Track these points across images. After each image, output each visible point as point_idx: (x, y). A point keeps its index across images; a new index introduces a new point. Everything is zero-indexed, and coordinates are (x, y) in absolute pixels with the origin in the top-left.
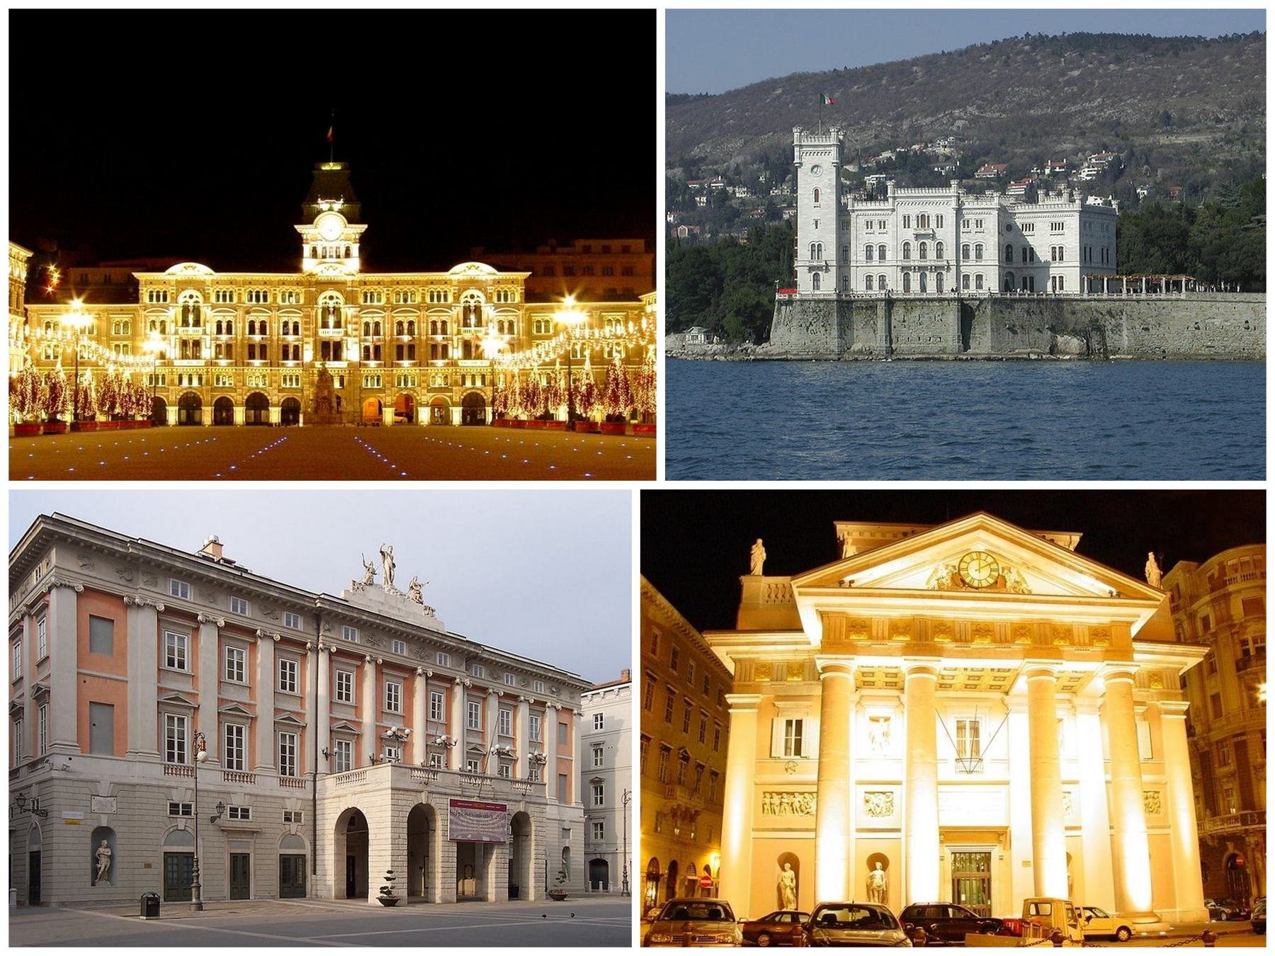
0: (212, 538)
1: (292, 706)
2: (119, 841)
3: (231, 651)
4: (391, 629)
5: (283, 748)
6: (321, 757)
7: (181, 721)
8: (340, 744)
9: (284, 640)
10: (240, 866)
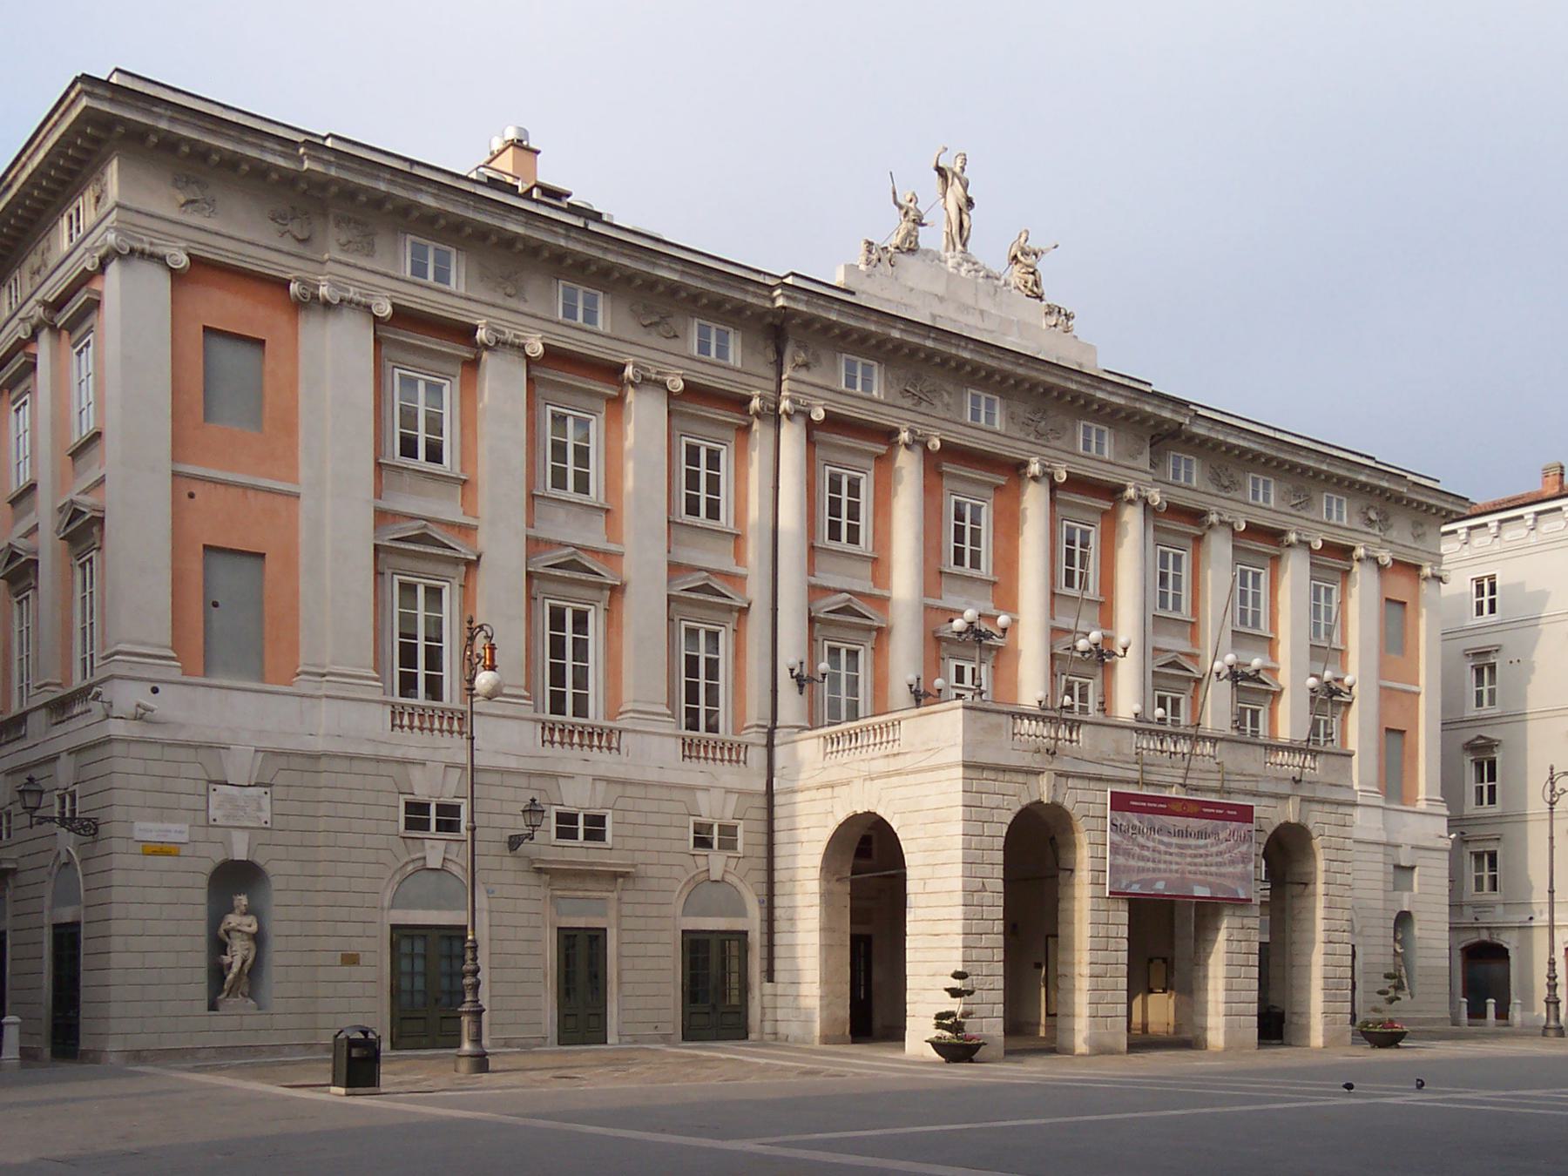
0: (511, 134)
2: (276, 898)
3: (559, 420)
4: (962, 363)
5: (692, 662)
6: (786, 684)
7: (434, 594)
8: (834, 652)
9: (694, 391)
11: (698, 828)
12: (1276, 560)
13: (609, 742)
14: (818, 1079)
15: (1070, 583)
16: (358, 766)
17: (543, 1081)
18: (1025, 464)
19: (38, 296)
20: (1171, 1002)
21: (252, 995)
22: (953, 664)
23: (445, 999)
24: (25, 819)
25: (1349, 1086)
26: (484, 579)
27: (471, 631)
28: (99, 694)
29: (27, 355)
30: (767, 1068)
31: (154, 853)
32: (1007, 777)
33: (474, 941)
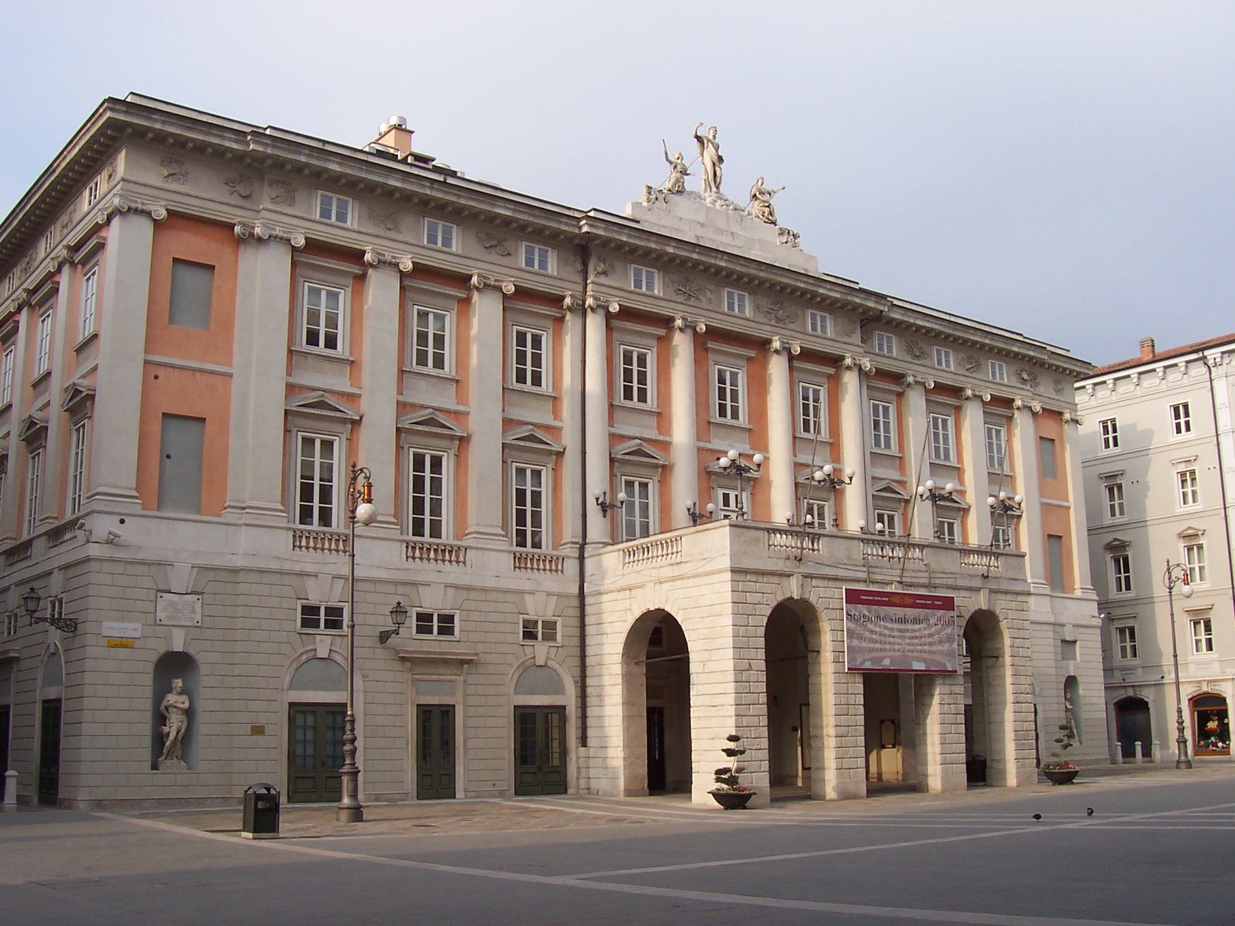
0: (394, 121)
1: (536, 414)
2: (204, 681)
3: (423, 316)
4: (719, 270)
5: (521, 494)
6: (593, 510)
7: (327, 446)
8: (629, 484)
9: (522, 293)
10: (436, 729)
11: (526, 624)
12: (958, 409)
13: (458, 557)
14: (623, 825)
15: (807, 429)
16: (267, 578)
17: (406, 829)
18: (769, 342)
19: (64, 243)
20: (899, 755)
21: (183, 758)
22: (720, 492)
23: (330, 763)
24: (27, 620)
25: (1038, 817)
26: (364, 432)
27: (354, 472)
28: (83, 525)
29: (53, 283)
30: (583, 816)
31: (116, 646)
32: (765, 579)
33: (352, 716)
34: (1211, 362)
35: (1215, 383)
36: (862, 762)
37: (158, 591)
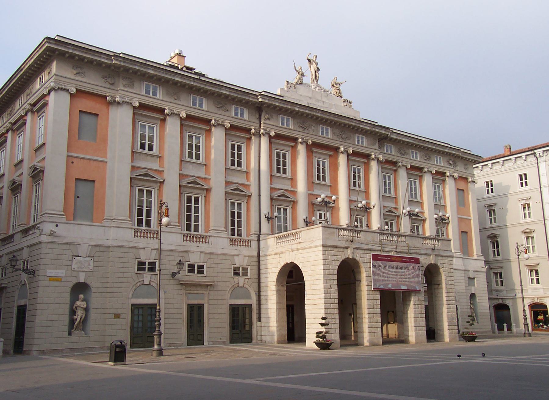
1: (239, 179)
2: (93, 295)
3: (191, 137)
4: (317, 117)
5: (233, 213)
7: (149, 193)
8: (279, 209)
10: (196, 314)
11: (235, 269)
12: (421, 177)
13: (206, 240)
14: (277, 356)
15: (355, 185)
17: (182, 359)
18: (339, 148)
19: (28, 102)
20: (396, 326)
21: (83, 329)
22: (318, 212)
24: (11, 270)
25: (459, 356)
26: (165, 187)
28: (38, 227)
30: (259, 352)
31: (53, 281)
32: (337, 250)
33: (159, 309)
34: (538, 155)
35: (540, 165)
36: (380, 329)
37: (73, 256)
